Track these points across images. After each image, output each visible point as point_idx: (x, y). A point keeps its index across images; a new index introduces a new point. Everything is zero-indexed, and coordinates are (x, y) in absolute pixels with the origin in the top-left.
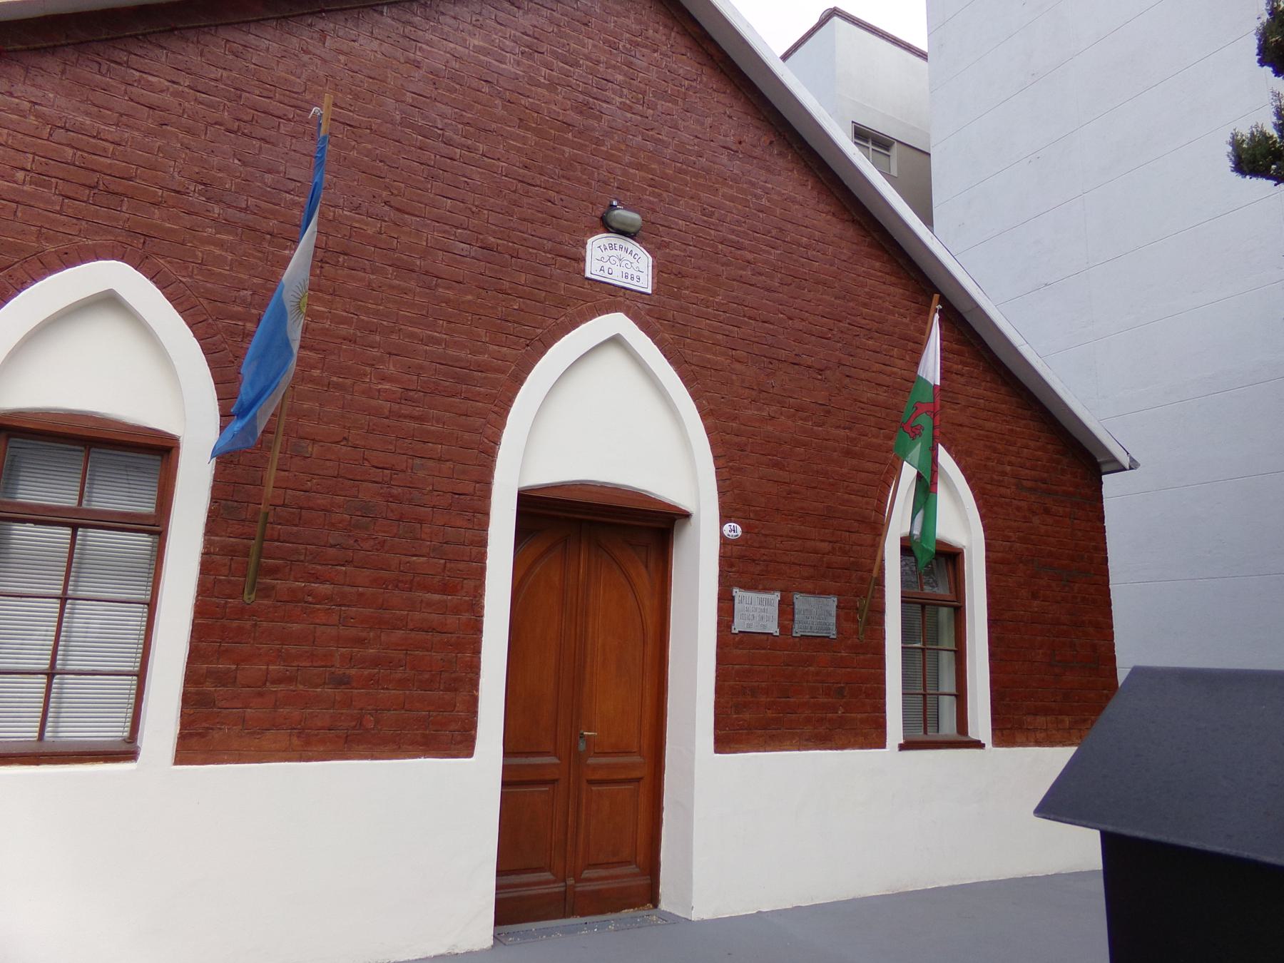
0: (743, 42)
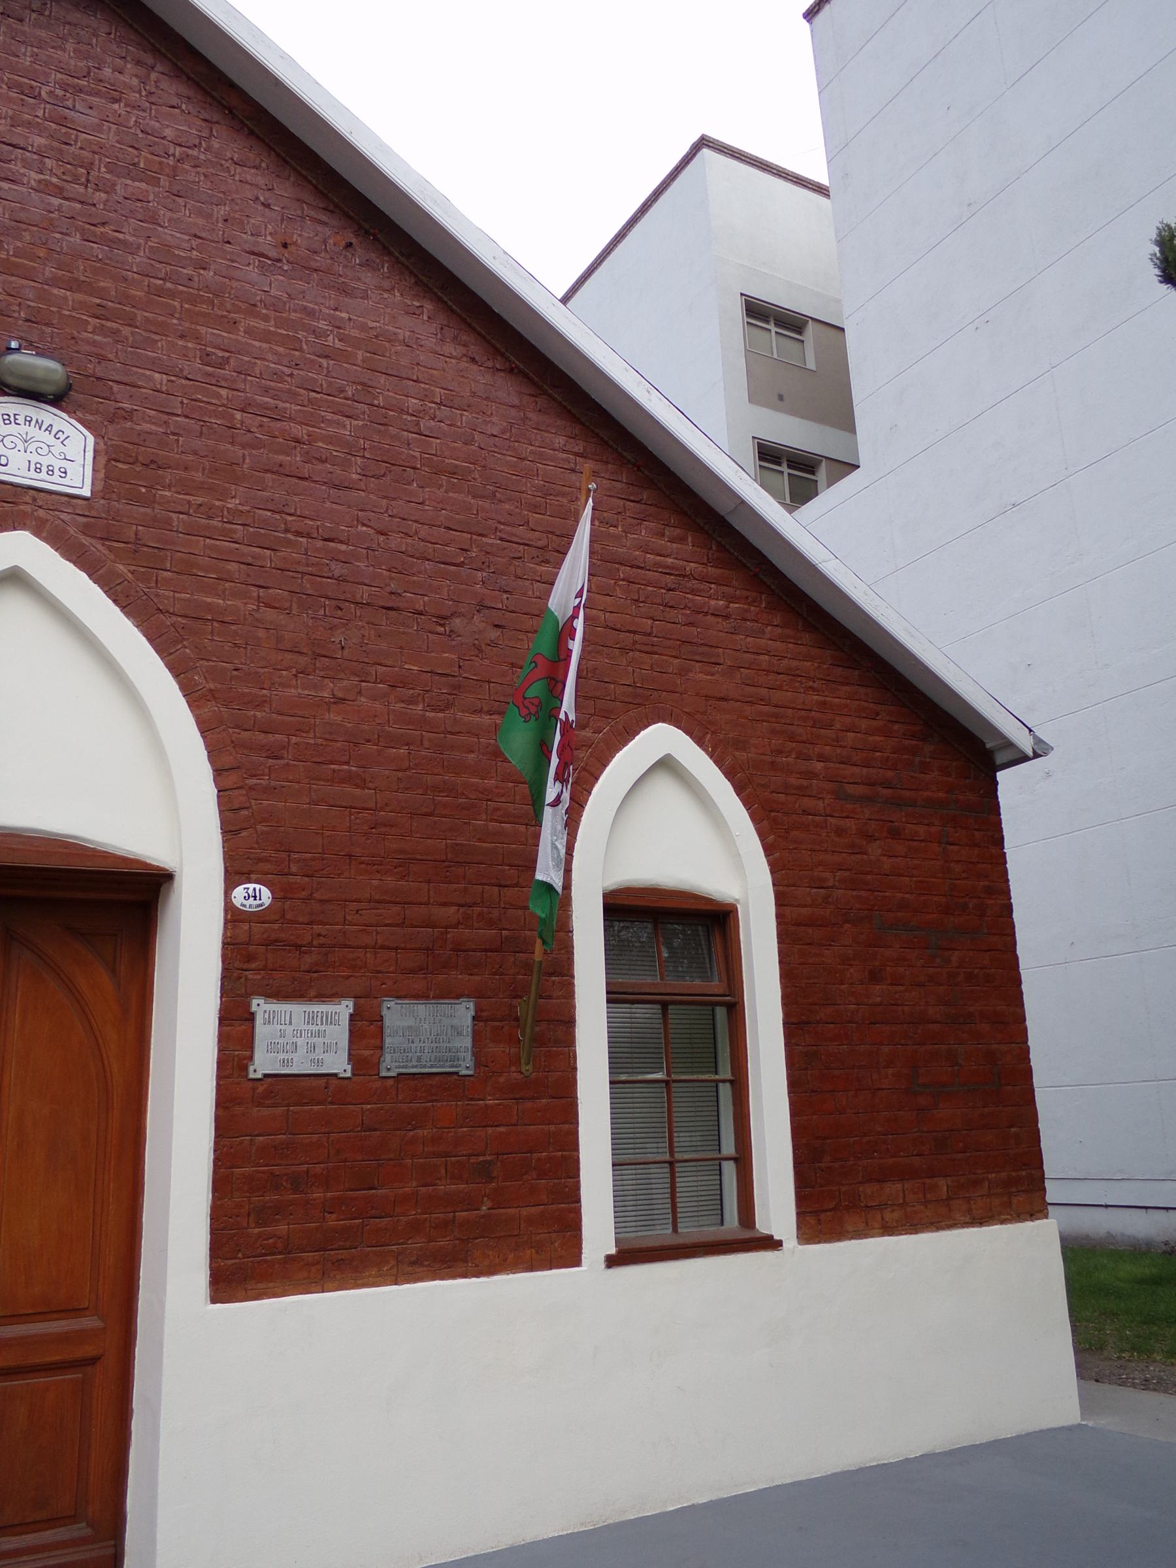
0: (277, 84)
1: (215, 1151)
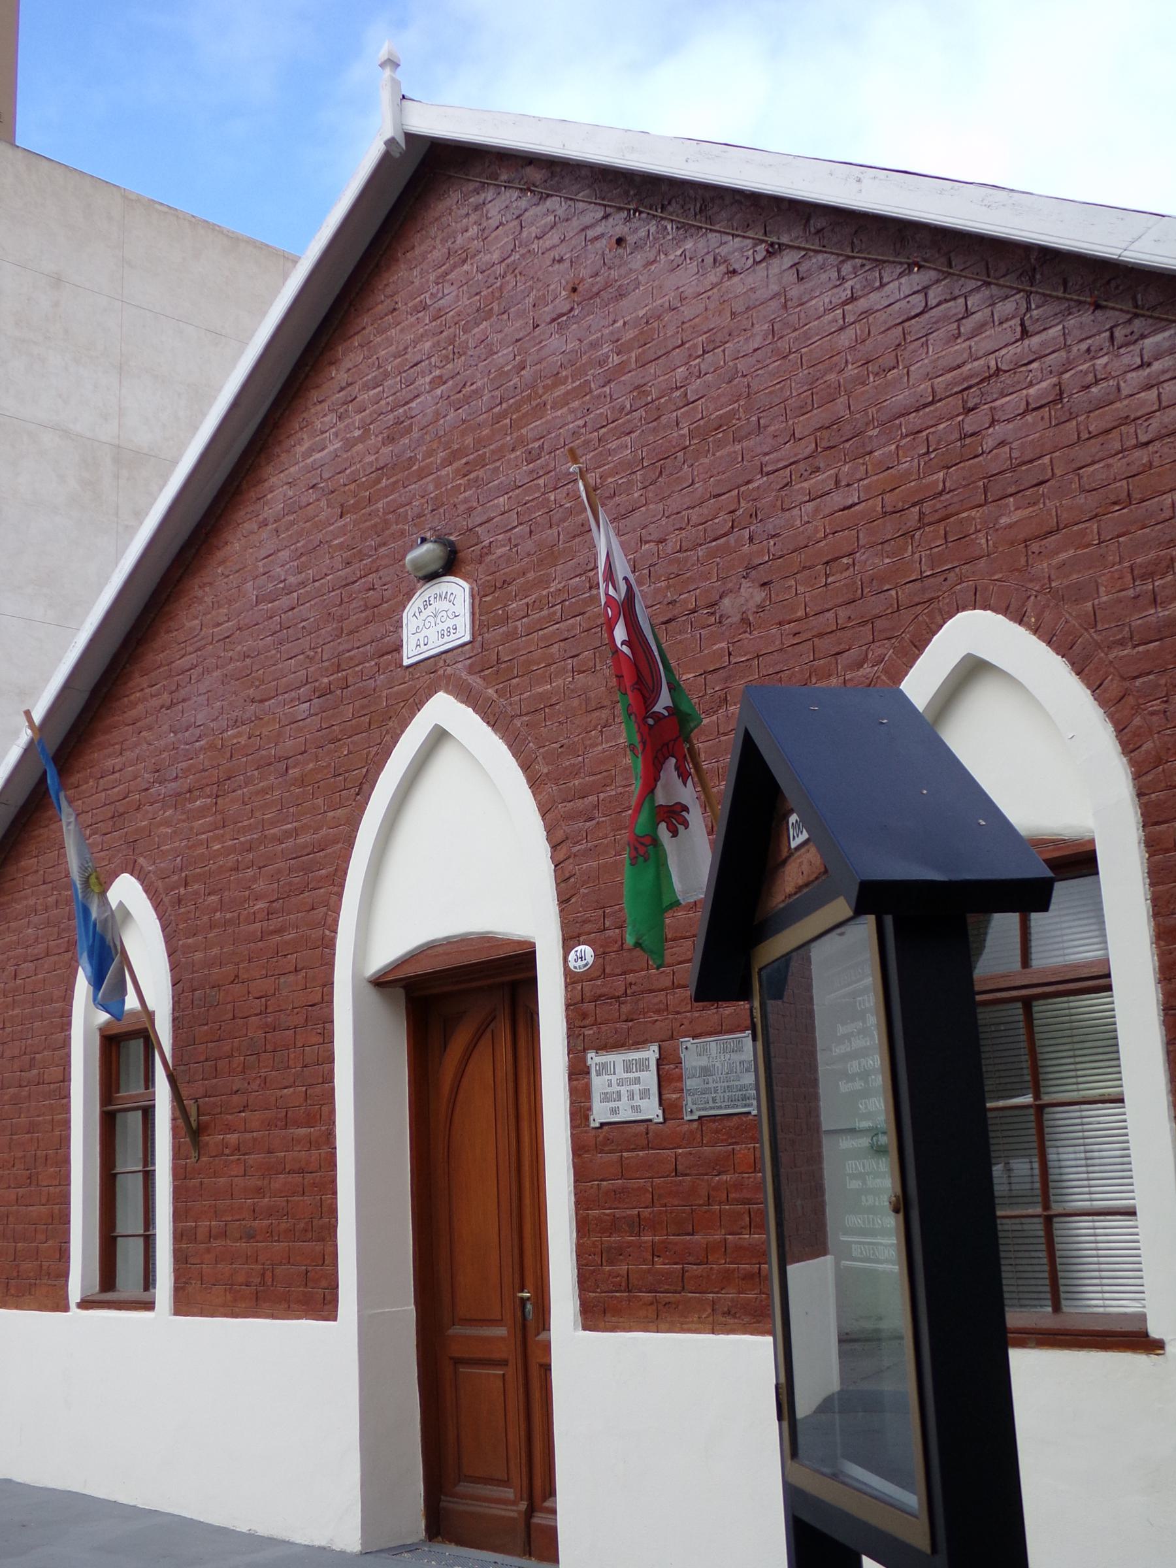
1: (575, 1194)
